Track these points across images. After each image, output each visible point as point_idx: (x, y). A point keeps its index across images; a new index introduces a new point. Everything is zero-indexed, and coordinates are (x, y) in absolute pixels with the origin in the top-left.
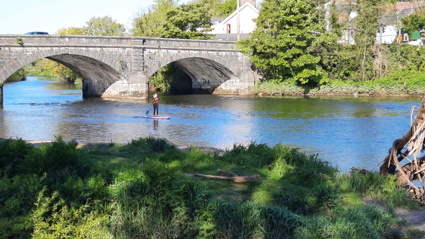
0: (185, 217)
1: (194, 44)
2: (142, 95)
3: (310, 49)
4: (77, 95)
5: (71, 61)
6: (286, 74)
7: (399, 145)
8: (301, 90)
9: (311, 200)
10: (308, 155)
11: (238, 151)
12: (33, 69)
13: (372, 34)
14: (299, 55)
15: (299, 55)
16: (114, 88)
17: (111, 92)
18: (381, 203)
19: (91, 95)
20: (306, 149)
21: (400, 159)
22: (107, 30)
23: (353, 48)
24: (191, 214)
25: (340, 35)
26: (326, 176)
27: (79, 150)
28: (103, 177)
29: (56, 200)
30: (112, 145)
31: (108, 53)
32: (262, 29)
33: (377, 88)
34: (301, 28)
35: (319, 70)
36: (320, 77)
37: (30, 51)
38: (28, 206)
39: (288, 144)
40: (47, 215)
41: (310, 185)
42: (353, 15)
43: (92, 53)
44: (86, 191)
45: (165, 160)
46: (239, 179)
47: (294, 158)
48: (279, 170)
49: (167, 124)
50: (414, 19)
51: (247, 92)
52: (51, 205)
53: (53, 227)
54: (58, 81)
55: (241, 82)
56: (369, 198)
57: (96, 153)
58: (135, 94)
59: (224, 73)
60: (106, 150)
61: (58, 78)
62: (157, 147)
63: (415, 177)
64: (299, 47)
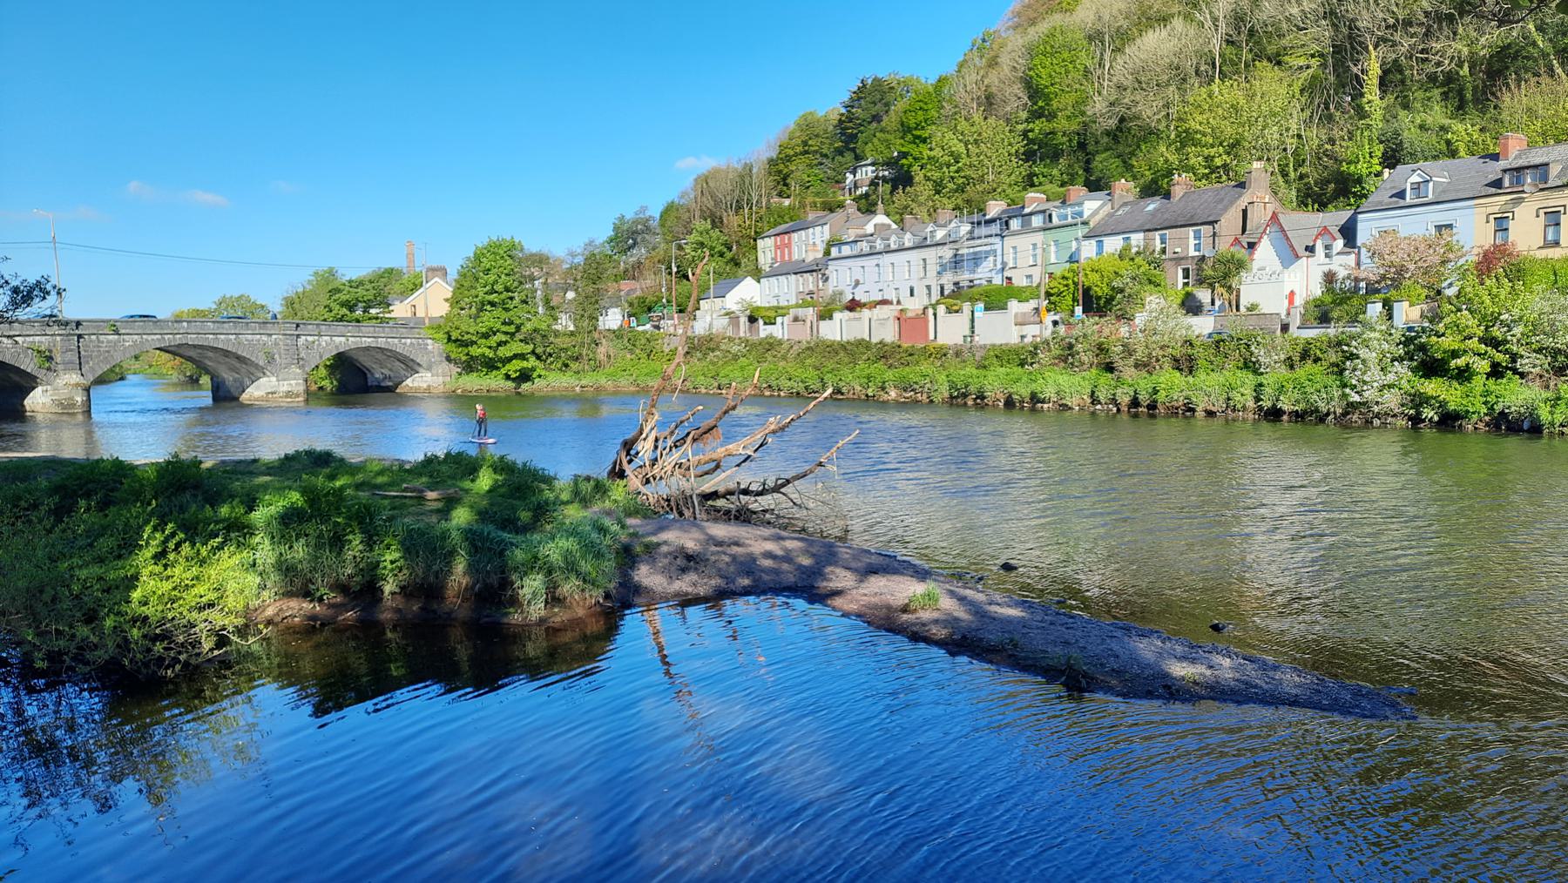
0: (361, 547)
1: (367, 328)
2: (298, 396)
3: (519, 336)
4: (205, 398)
5: (192, 353)
6: (491, 365)
7: (628, 446)
8: (510, 384)
9: (525, 516)
10: (519, 462)
11: (430, 461)
12: (137, 365)
13: (594, 318)
14: (505, 343)
15: (505, 343)
16: (258, 388)
17: (254, 392)
18: (609, 513)
19: (225, 397)
20: (518, 457)
21: (630, 462)
22: (241, 313)
23: (572, 334)
24: (369, 543)
25: (556, 319)
26: (543, 486)
27: (208, 470)
28: (242, 502)
29: (173, 535)
30: (255, 461)
31: (247, 341)
32: (456, 311)
33: (603, 381)
34: (507, 310)
35: (532, 362)
36: (533, 369)
37: (129, 341)
38: (129, 546)
39: (494, 452)
40: (160, 556)
41: (523, 498)
42: (570, 295)
43: (222, 342)
44: (217, 522)
45: (332, 477)
46: (431, 495)
47: (503, 466)
48: (485, 481)
49: (329, 432)
50: (642, 300)
51: (441, 389)
52: (165, 542)
53: (169, 572)
54: (175, 380)
55: (432, 377)
56: (596, 508)
57: (233, 472)
58: (288, 394)
59: (411, 366)
60: (250, 467)
61: (175, 376)
62: (321, 460)
63: (648, 481)
64: (506, 333)
